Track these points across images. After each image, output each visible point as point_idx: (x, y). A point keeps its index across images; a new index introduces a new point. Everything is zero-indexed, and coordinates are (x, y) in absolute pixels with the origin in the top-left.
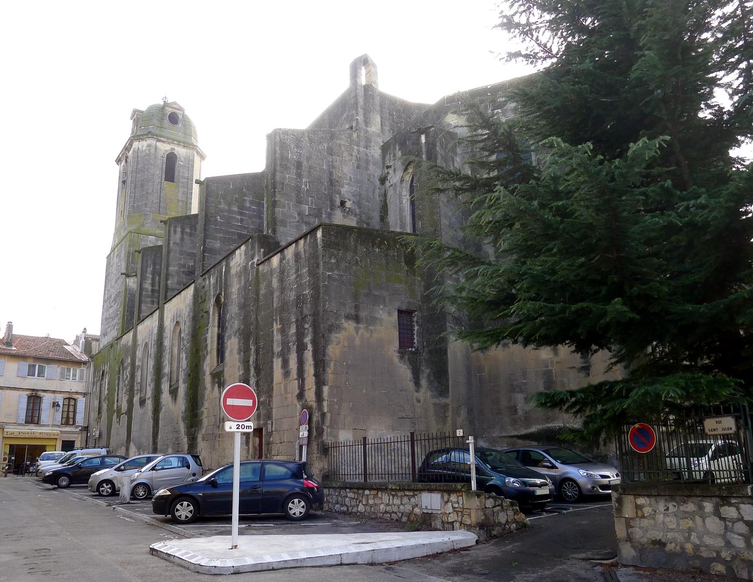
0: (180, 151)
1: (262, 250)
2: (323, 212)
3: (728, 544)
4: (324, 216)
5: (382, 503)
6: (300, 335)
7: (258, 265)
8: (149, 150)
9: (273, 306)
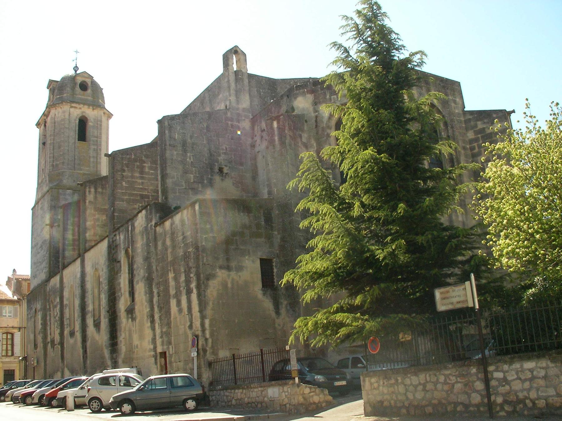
0: (90, 113)
1: (158, 215)
2: (205, 178)
3: (407, 398)
4: (205, 181)
5: (246, 397)
6: (188, 281)
7: (156, 226)
8: (64, 116)
9: (167, 260)
